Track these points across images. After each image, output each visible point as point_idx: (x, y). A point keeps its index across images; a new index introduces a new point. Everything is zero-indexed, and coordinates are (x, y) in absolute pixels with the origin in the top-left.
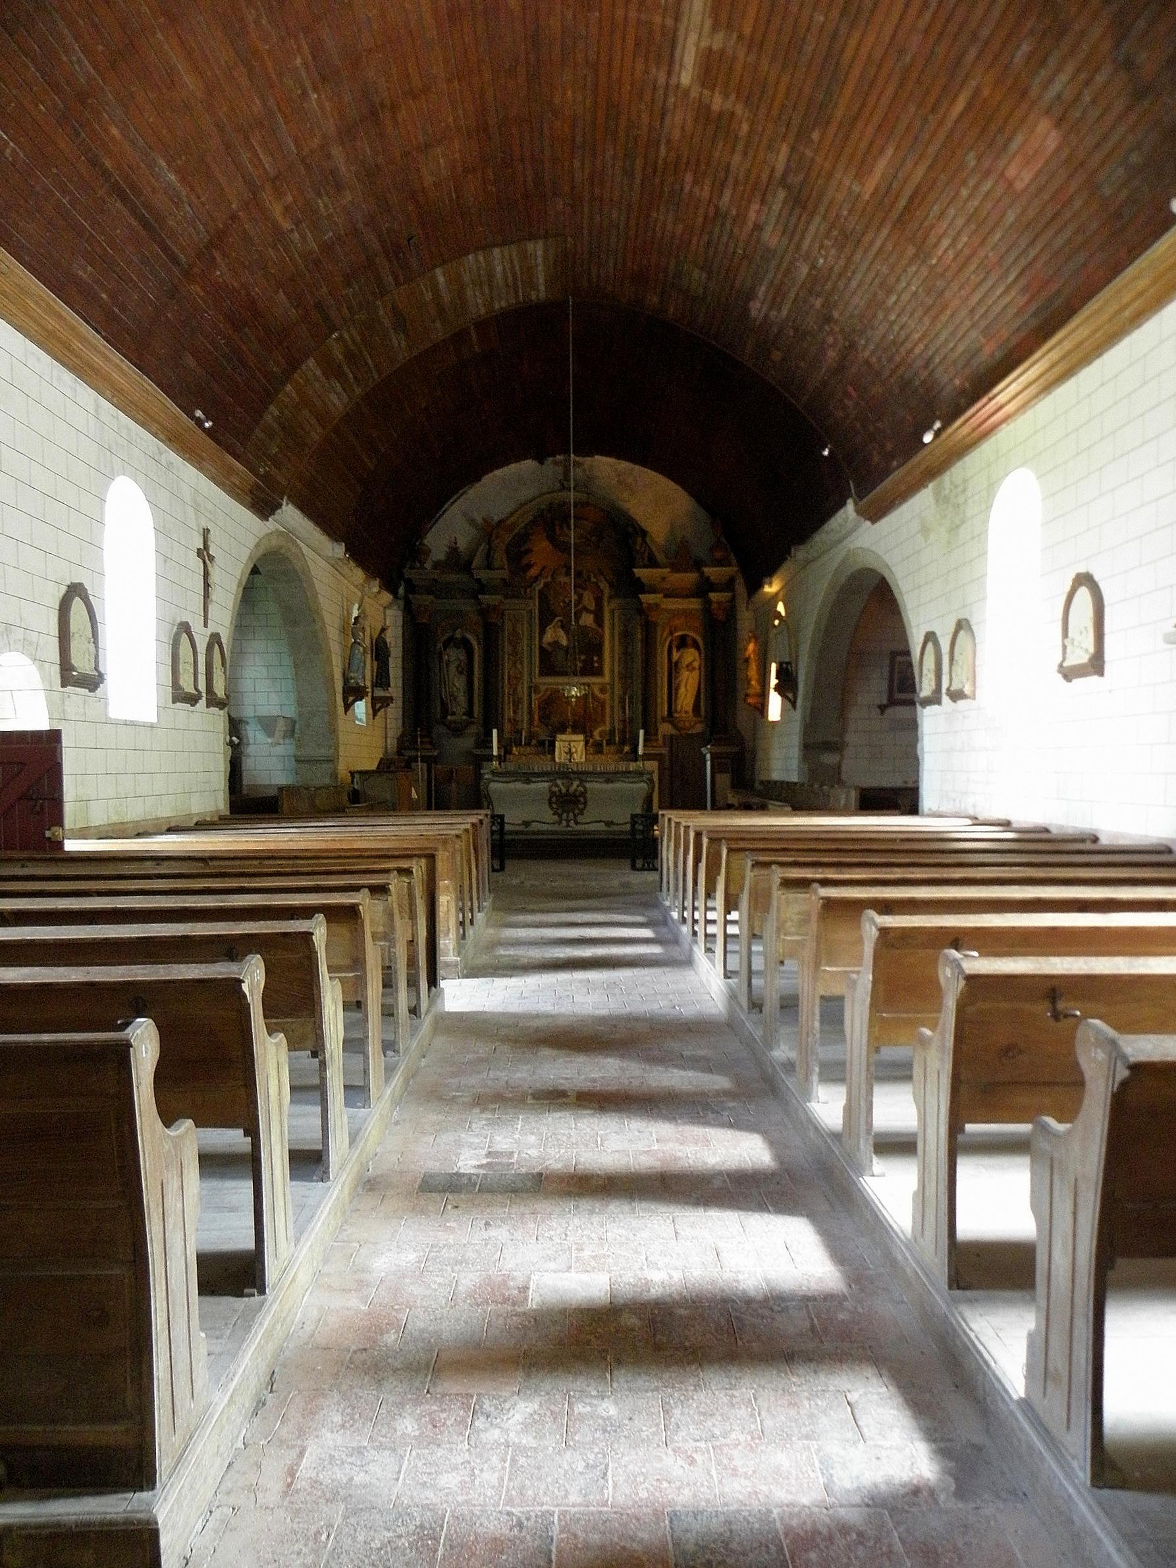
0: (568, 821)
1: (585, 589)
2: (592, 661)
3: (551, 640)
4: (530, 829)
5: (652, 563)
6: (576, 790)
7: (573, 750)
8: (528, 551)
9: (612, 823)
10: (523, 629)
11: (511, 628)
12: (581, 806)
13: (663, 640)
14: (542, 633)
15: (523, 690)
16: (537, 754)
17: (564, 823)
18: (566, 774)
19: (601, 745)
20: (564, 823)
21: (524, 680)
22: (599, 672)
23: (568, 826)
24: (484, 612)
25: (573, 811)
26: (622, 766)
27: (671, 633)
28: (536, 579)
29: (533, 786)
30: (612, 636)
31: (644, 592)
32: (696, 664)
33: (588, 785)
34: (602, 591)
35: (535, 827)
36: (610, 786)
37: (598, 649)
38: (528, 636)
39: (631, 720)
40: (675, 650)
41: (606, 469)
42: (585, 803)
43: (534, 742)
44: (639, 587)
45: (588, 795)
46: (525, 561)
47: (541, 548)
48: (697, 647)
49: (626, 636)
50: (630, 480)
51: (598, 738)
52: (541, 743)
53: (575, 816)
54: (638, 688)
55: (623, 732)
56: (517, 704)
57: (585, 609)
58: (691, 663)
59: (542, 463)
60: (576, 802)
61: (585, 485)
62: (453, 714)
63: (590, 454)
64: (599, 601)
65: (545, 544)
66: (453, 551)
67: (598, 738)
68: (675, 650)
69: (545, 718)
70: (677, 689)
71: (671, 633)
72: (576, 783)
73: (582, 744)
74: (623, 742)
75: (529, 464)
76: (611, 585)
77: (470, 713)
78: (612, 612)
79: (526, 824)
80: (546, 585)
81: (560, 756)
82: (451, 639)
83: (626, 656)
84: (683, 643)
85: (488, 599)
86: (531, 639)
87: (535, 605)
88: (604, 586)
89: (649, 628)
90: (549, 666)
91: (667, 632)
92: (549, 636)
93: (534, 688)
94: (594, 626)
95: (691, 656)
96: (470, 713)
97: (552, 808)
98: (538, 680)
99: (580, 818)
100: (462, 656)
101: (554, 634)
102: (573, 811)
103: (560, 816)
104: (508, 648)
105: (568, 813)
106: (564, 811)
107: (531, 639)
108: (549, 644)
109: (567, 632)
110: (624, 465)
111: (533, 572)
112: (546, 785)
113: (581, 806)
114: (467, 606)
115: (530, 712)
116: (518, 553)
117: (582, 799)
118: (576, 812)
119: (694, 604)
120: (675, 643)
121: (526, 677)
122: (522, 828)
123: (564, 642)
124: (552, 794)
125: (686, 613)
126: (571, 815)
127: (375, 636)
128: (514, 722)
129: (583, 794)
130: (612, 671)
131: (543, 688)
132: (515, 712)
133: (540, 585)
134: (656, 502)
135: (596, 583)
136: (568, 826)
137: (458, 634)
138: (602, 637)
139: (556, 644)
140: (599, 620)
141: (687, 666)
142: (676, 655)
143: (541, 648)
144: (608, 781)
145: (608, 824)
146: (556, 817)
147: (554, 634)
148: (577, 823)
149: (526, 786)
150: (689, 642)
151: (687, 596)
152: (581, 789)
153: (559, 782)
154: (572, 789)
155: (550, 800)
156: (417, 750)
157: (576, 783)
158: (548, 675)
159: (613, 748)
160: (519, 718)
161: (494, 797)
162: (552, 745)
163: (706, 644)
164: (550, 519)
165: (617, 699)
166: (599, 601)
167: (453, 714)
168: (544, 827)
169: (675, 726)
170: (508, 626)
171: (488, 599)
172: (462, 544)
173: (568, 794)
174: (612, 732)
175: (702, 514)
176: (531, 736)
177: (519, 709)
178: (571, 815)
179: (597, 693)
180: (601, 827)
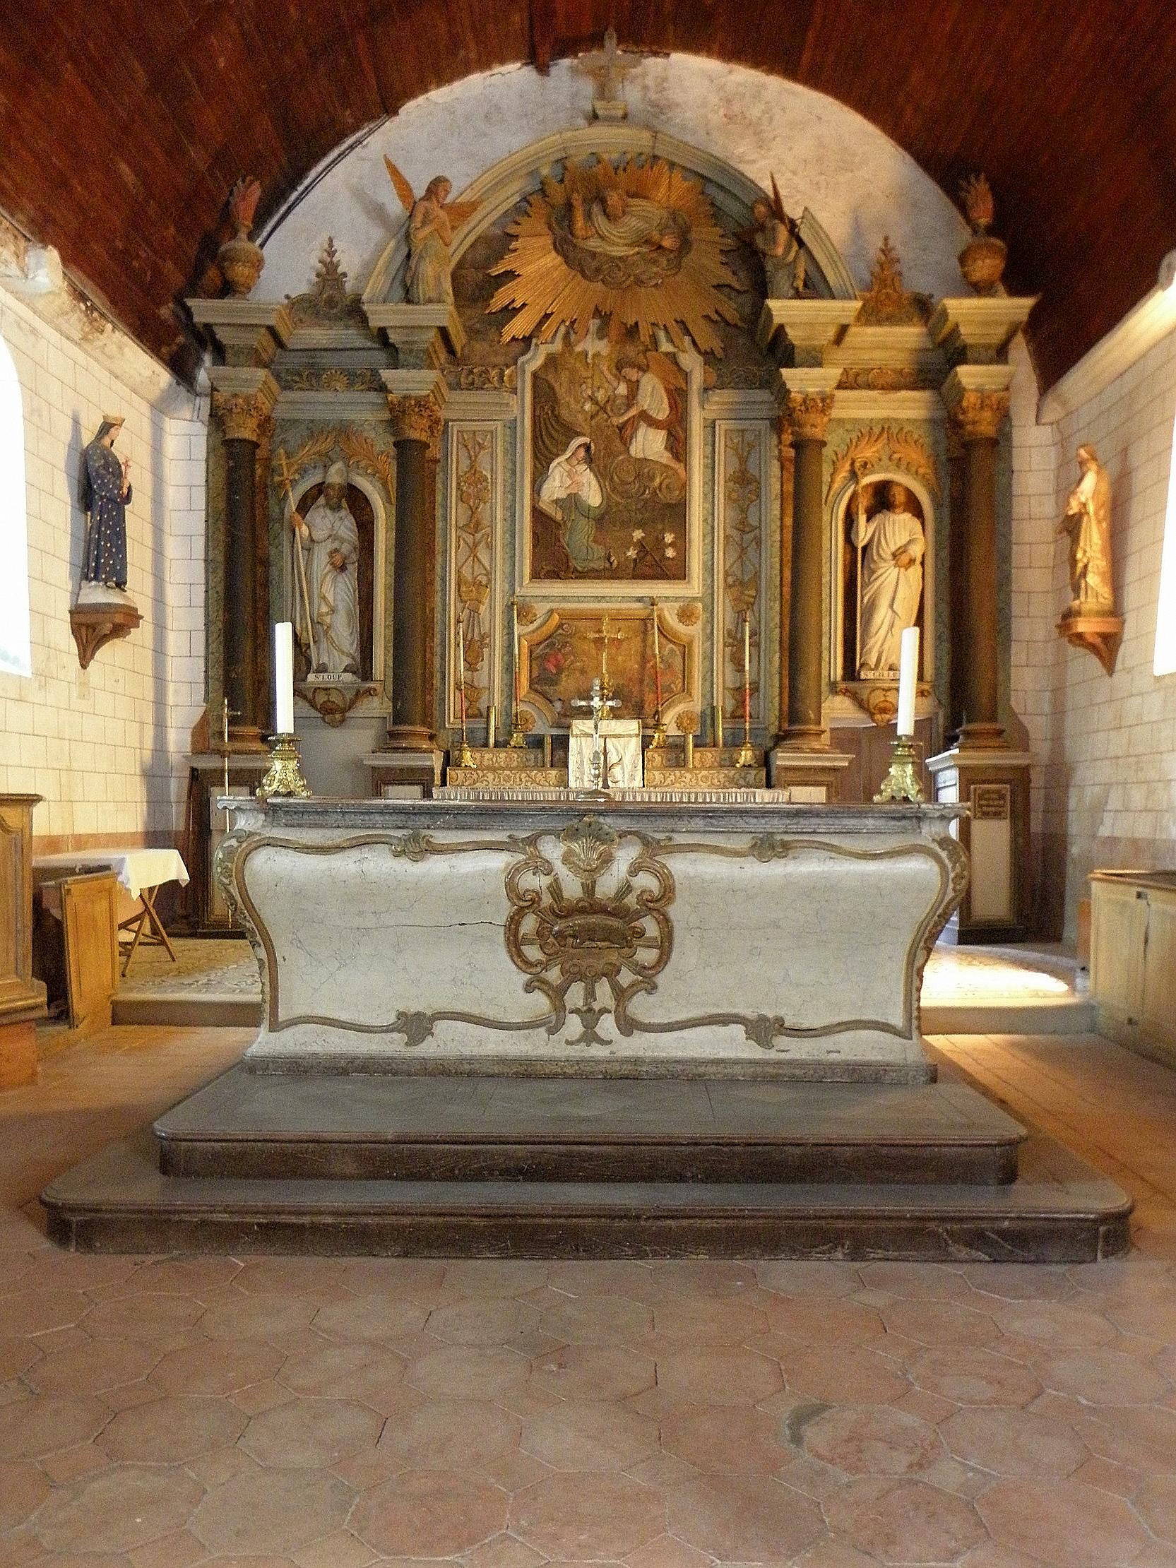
0: (590, 1016)
1: (644, 369)
2: (660, 544)
3: (562, 494)
4: (428, 1048)
5: (814, 287)
6: (627, 889)
7: (613, 758)
8: (510, 275)
9: (780, 1027)
10: (494, 466)
11: (465, 463)
12: (647, 956)
13: (837, 493)
14: (540, 476)
15: (492, 614)
16: (524, 767)
17: (574, 1025)
18: (588, 819)
19: (682, 748)
20: (574, 1025)
21: (495, 595)
22: (678, 572)
23: (590, 1036)
24: (397, 416)
25: (611, 973)
26: (738, 797)
27: (854, 476)
28: (526, 342)
29: (436, 866)
30: (710, 482)
31: (790, 363)
32: (916, 551)
33: (679, 866)
34: (686, 376)
35: (449, 1041)
36: (777, 870)
37: (676, 513)
38: (501, 481)
39: (755, 689)
40: (862, 518)
41: (701, 93)
42: (665, 945)
43: (517, 738)
44: (779, 350)
45: (675, 911)
46: (499, 300)
47: (537, 268)
48: (915, 508)
49: (745, 483)
50: (755, 112)
51: (672, 731)
52: (538, 743)
53: (621, 995)
54: (771, 611)
55: (736, 716)
56: (474, 651)
57: (644, 417)
58: (903, 550)
59: (543, 70)
60: (628, 938)
61: (655, 115)
62: (322, 669)
63: (658, 45)
64: (678, 398)
65: (552, 260)
66: (330, 274)
67: (672, 731)
68: (862, 518)
69: (543, 682)
70: (871, 608)
71: (854, 476)
72: (626, 856)
73: (635, 744)
74: (599, 836)
75: (513, 75)
76: (708, 357)
77: (364, 668)
78: (711, 426)
79: (415, 1025)
80: (551, 361)
81: (581, 775)
82: (320, 489)
83: (745, 533)
84: (882, 500)
85: (407, 381)
86: (512, 489)
87: (522, 407)
88: (691, 361)
89: (803, 454)
90: (553, 560)
91: (843, 473)
92: (557, 484)
93: (518, 610)
94: (666, 458)
95: (901, 531)
96: (364, 668)
97: (523, 963)
98: (529, 589)
99: (640, 1006)
100: (345, 526)
101: (572, 480)
102: (611, 973)
103: (557, 994)
104: (456, 513)
105: (590, 982)
106: (572, 976)
107: (512, 489)
108: (556, 501)
109: (602, 475)
110: (743, 76)
111: (519, 326)
112: (498, 862)
113: (647, 956)
114: (362, 411)
115: (509, 668)
116: (479, 282)
117: (650, 926)
118: (626, 977)
119: (911, 407)
120: (863, 503)
121: (499, 585)
122: (393, 1046)
123: (593, 496)
124: (524, 903)
125: (886, 430)
126: (604, 990)
127: (87, 438)
128: (470, 691)
129: (658, 904)
130: (709, 569)
131: (541, 609)
132: (471, 667)
133: (534, 361)
134: (823, 159)
135: (673, 358)
136: (590, 1036)
137: (335, 475)
138: (685, 486)
139: (572, 503)
140: (678, 446)
141: (894, 555)
142: (864, 532)
143: (538, 514)
144: (767, 848)
145: (764, 1029)
146: (540, 1003)
147: (572, 480)
148: (628, 1026)
149: (406, 868)
150: (900, 497)
151: (895, 387)
152: (645, 881)
153: (552, 850)
154: (608, 885)
155: (513, 924)
156: (222, 754)
157: (626, 856)
158: (554, 575)
159: (709, 755)
160: (482, 679)
161: (270, 913)
162: (562, 743)
163: (937, 506)
164: (568, 197)
165: (719, 637)
166: (678, 398)
167: (322, 669)
168: (494, 1044)
169: (862, 705)
170: (457, 464)
171: (407, 381)
172: (349, 262)
173: (589, 905)
174: (709, 717)
175: (929, 189)
176: (513, 722)
177: (481, 666)
178: (604, 990)
179: (672, 620)
180: (731, 1044)
